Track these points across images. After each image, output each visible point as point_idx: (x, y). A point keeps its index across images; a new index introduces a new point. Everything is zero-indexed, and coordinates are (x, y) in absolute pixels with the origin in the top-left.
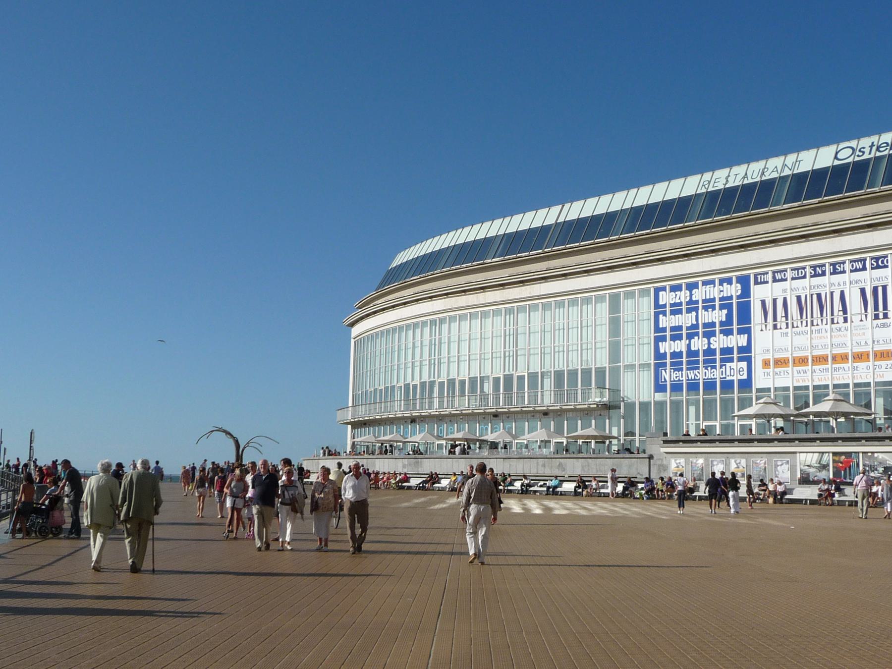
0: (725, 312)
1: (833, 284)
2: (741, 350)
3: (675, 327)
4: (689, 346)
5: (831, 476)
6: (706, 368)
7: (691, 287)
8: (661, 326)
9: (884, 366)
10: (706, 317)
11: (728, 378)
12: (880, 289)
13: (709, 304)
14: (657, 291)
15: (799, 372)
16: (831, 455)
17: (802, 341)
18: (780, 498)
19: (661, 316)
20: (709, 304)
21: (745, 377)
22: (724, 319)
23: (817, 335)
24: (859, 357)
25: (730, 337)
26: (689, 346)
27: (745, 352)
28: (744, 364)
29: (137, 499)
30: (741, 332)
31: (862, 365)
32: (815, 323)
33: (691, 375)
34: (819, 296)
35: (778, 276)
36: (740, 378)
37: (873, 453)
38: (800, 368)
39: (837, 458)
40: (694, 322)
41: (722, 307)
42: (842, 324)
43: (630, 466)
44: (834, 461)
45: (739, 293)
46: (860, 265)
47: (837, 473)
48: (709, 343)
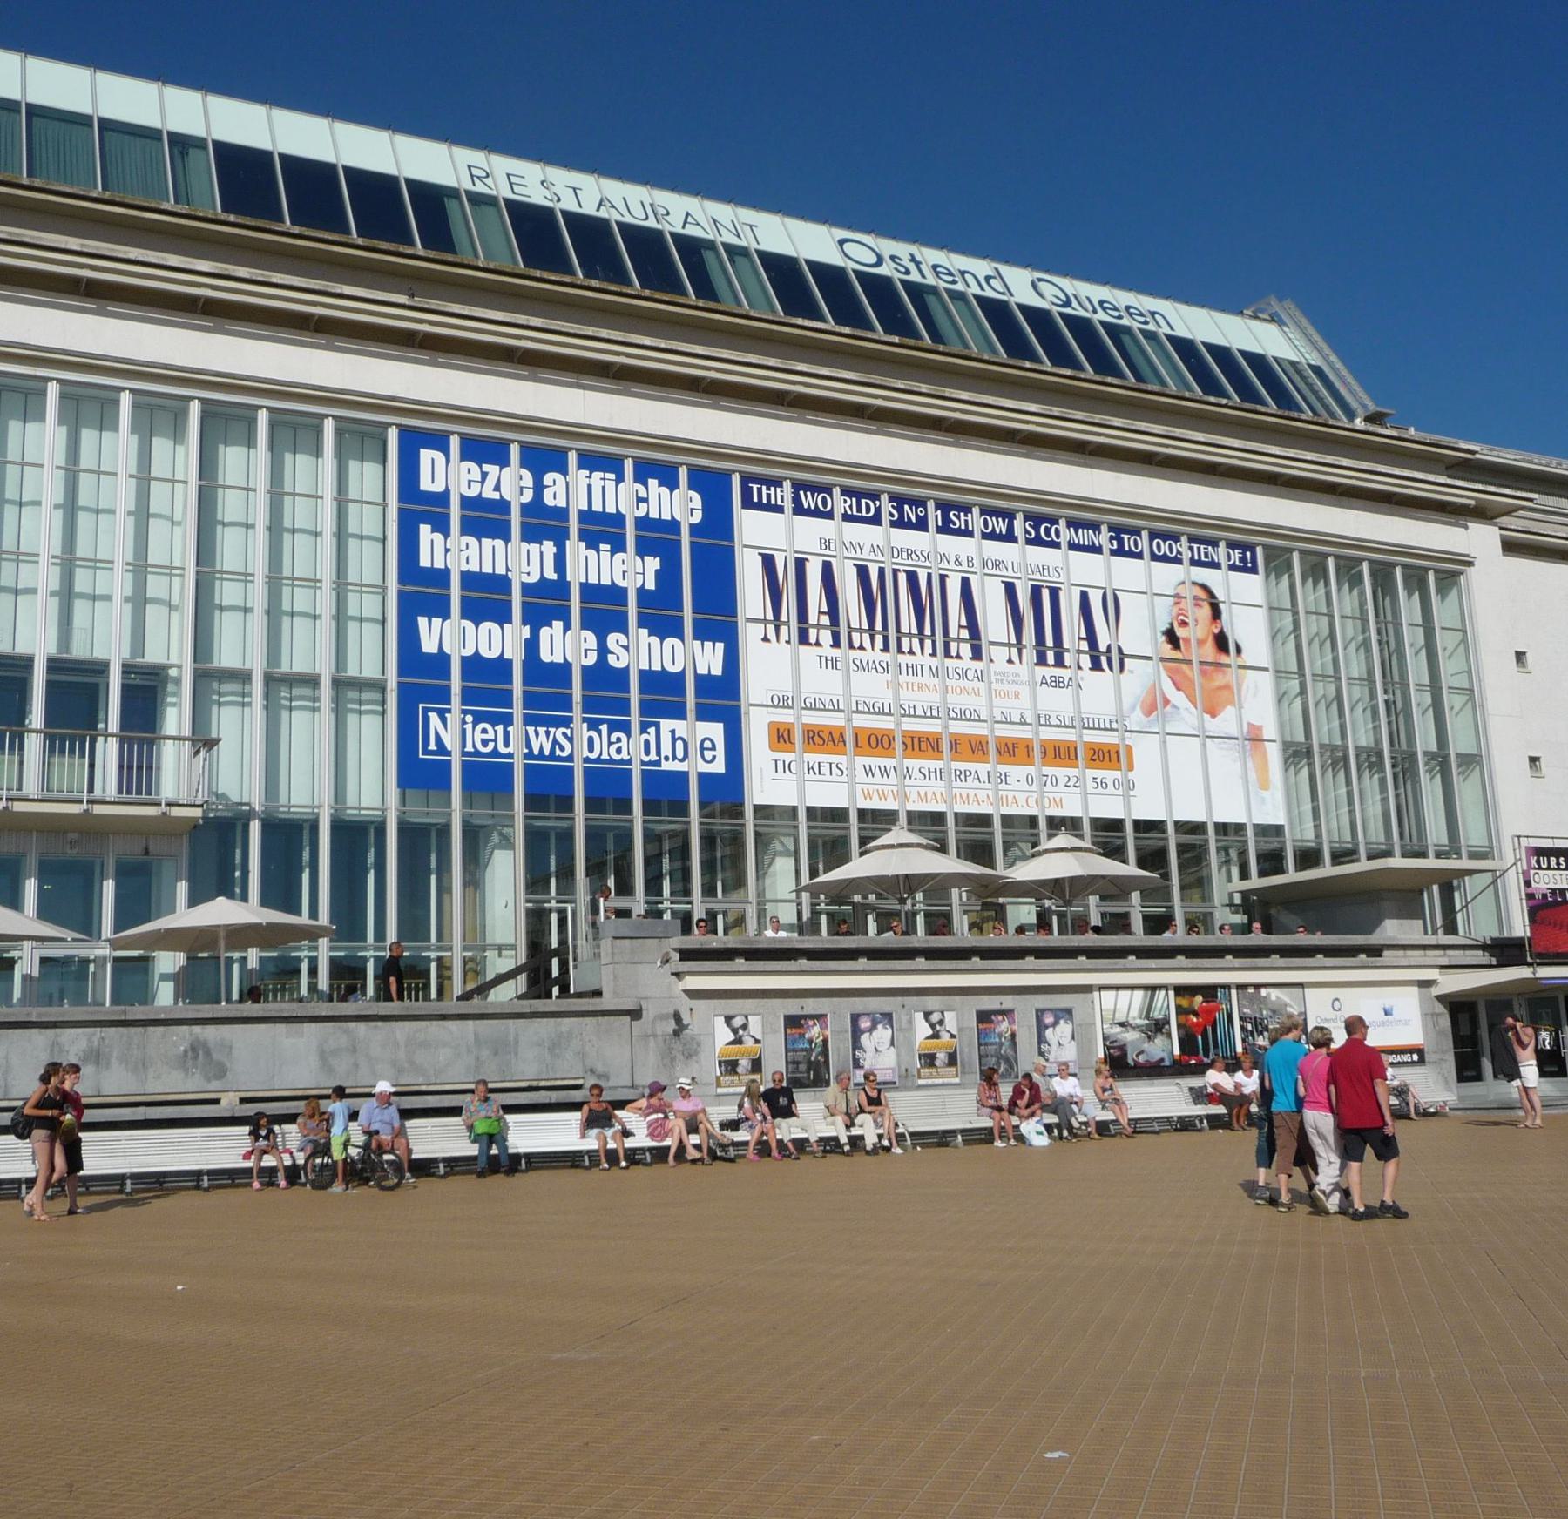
0: (653, 563)
1: (943, 557)
2: (705, 684)
3: (599, 587)
4: (532, 646)
5: (1177, 1051)
6: (594, 725)
7: (543, 460)
8: (425, 562)
9: (1062, 781)
10: (589, 565)
11: (666, 766)
12: (1046, 594)
13: (602, 529)
14: (413, 442)
15: (869, 772)
16: (1172, 993)
17: (872, 687)
18: (718, 1154)
19: (425, 530)
20: (602, 529)
21: (719, 767)
22: (651, 585)
23: (911, 678)
24: (1011, 751)
25: (669, 641)
26: (532, 646)
27: (722, 697)
28: (716, 731)
29: (329, 1131)
30: (702, 633)
31: (1017, 772)
32: (906, 648)
33: (541, 741)
34: (912, 578)
35: (808, 500)
36: (704, 768)
37: (1258, 986)
38: (874, 762)
39: (1184, 1002)
40: (551, 575)
41: (643, 549)
42: (967, 662)
43: (555, 1046)
44: (1180, 1010)
45: (697, 517)
46: (1000, 526)
47: (1187, 1043)
48: (603, 650)
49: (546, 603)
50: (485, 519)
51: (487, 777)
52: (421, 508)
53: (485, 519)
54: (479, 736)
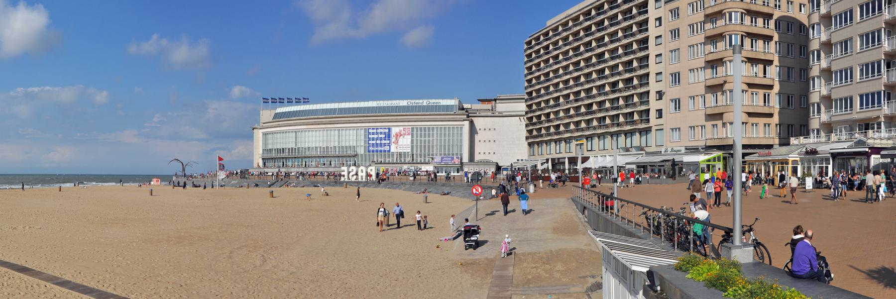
10: (380, 136)
13: (381, 133)
20: (381, 133)
49: (377, 139)
50: (373, 134)
51: (373, 151)
52: (369, 133)
53: (373, 134)
54: (737, 85)
